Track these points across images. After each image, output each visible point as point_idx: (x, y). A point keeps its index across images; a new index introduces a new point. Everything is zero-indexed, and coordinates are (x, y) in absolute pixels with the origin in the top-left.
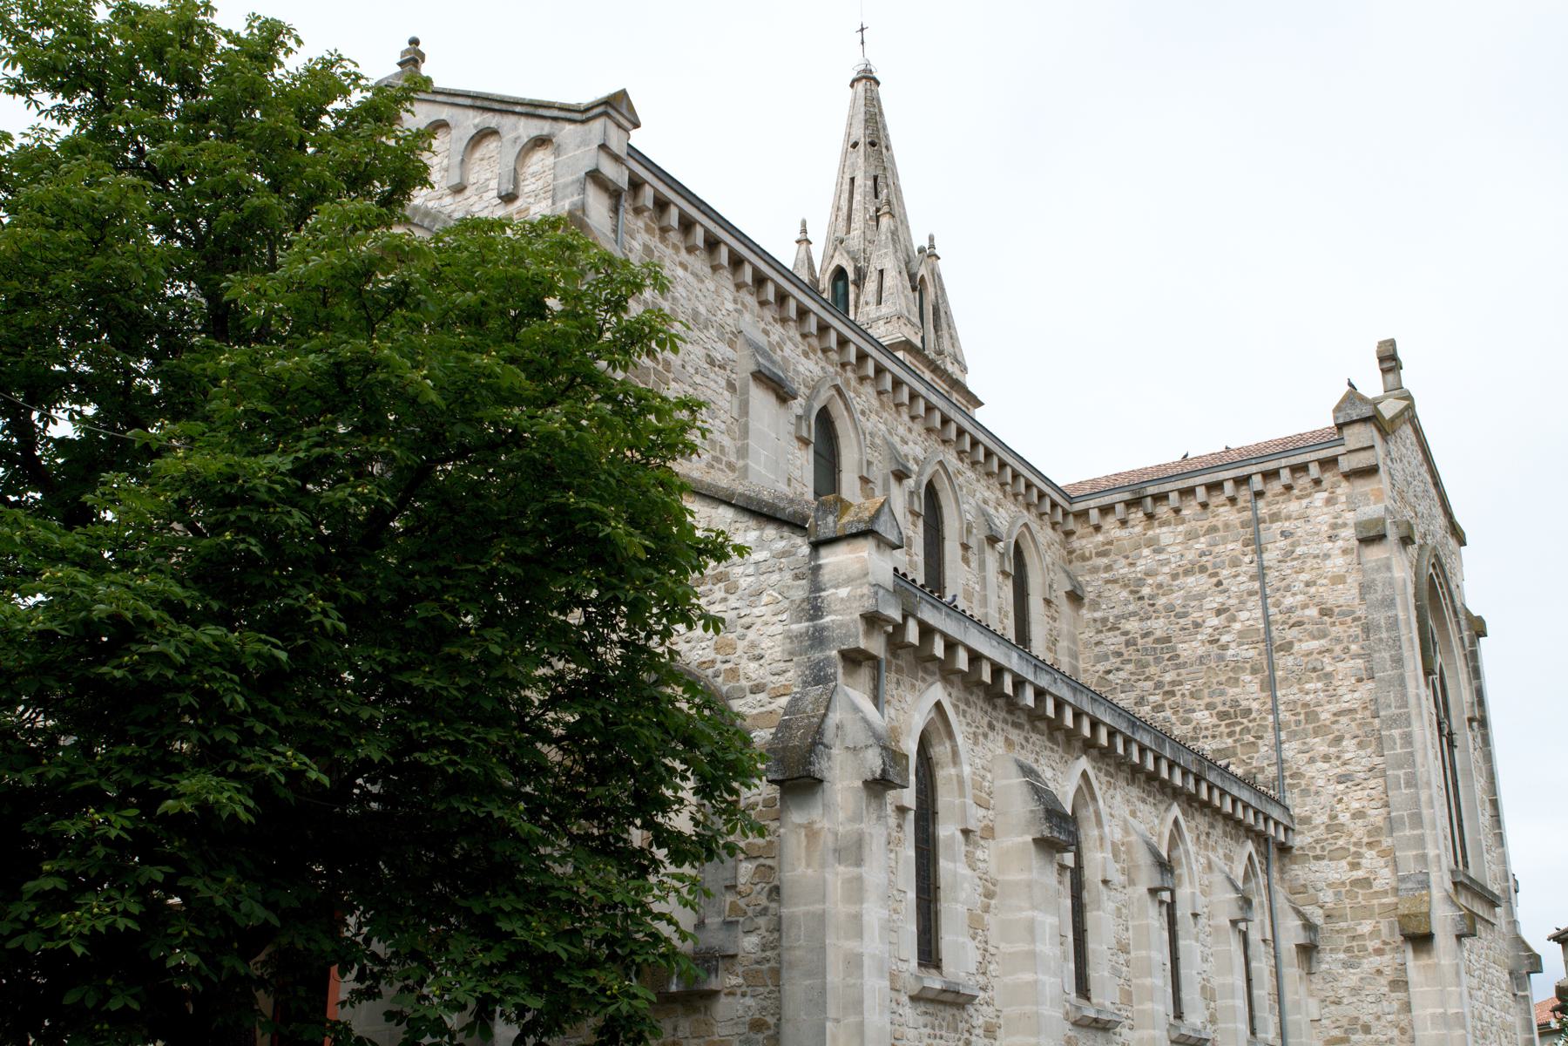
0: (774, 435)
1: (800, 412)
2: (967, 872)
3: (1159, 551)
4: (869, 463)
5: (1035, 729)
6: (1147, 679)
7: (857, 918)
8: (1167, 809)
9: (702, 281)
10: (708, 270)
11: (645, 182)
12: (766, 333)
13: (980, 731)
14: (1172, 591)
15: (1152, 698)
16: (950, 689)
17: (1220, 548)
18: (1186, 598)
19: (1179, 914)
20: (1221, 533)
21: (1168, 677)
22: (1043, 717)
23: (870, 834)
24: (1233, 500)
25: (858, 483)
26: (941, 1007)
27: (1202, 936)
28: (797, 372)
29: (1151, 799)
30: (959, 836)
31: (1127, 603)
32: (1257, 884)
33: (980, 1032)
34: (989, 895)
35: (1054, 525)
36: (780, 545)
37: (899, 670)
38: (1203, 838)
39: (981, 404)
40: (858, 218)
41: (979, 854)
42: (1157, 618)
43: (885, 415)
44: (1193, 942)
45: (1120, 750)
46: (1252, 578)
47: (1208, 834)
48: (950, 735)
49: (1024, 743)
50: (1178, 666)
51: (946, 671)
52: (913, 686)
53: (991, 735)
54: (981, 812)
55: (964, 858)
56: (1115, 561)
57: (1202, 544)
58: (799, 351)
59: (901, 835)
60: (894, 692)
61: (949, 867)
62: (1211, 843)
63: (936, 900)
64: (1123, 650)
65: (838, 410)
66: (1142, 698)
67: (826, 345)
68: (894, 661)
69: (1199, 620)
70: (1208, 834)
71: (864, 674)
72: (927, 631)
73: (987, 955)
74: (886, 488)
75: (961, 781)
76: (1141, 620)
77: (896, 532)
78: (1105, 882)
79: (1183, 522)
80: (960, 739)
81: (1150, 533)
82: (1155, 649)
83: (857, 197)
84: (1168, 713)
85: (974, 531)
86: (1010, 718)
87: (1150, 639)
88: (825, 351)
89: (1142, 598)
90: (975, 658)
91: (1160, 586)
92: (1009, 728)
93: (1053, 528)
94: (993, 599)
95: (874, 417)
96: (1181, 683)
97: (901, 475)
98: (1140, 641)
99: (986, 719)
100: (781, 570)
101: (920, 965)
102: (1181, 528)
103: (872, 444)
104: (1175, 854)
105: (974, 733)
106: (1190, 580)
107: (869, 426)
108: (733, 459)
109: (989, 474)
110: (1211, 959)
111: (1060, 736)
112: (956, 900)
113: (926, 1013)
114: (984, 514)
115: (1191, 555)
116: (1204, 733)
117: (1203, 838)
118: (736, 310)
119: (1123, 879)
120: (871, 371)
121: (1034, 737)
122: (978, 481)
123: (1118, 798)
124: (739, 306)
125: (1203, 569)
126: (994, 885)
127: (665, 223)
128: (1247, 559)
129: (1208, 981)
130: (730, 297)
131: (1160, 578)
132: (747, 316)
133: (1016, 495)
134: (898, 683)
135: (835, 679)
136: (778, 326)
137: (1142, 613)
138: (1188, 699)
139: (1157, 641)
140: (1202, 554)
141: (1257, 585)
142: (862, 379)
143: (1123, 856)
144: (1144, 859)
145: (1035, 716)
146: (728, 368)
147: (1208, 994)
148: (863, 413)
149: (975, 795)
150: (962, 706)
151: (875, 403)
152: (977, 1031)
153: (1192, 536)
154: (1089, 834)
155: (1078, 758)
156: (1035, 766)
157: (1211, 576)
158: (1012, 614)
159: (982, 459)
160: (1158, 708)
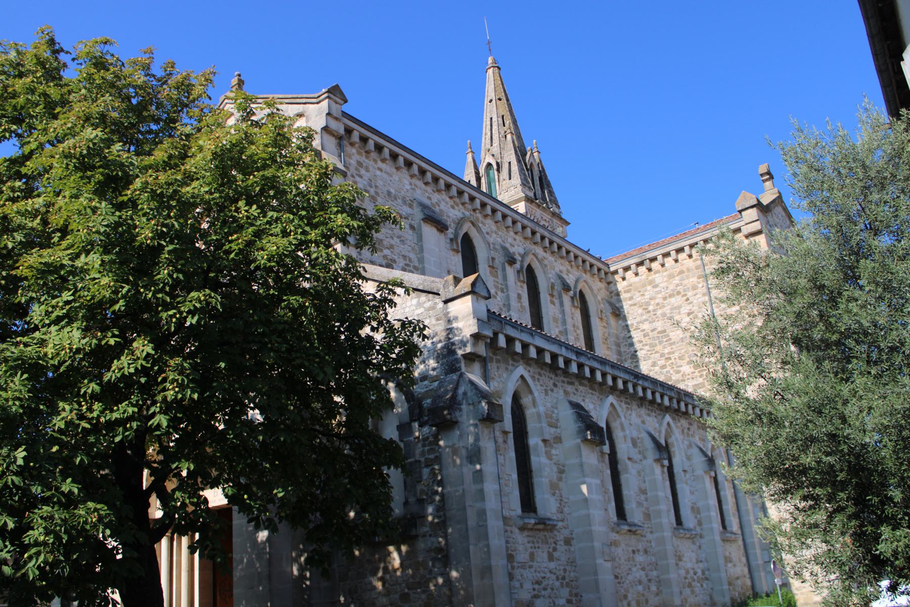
0: (437, 250)
1: (452, 236)
2: (547, 462)
3: (656, 286)
4: (493, 259)
5: (581, 384)
6: (656, 352)
7: (481, 491)
8: (663, 418)
9: (391, 176)
10: (394, 170)
11: (354, 129)
12: (429, 198)
13: (549, 388)
14: (664, 306)
15: (659, 363)
16: (528, 368)
17: (685, 282)
18: (671, 309)
19: (675, 471)
20: (686, 274)
21: (666, 351)
22: (584, 378)
23: (485, 447)
24: (690, 256)
25: (488, 269)
26: (538, 532)
27: (689, 482)
28: (449, 217)
29: (653, 414)
30: (541, 444)
31: (642, 315)
32: (720, 451)
33: (562, 543)
34: (561, 472)
35: (601, 280)
36: (428, 304)
37: (498, 361)
38: (686, 431)
39: (569, 224)
40: (496, 136)
41: (554, 452)
42: (658, 321)
43: (500, 233)
44: (684, 485)
45: (631, 390)
46: (704, 295)
47: (689, 429)
48: (531, 392)
49: (575, 392)
50: (671, 344)
51: (524, 357)
52: (507, 369)
53: (555, 390)
54: (553, 430)
55: (544, 455)
56: (634, 295)
57: (676, 280)
58: (449, 206)
59: (506, 446)
60: (496, 373)
61: (538, 460)
62: (691, 433)
63: (531, 477)
64: (643, 339)
65: (474, 234)
66: (655, 362)
67: (463, 201)
68: (494, 357)
69: (679, 320)
70: (689, 429)
71: (477, 366)
72: (510, 340)
73: (562, 503)
74: (504, 269)
75: (539, 415)
76: (650, 323)
77: (485, 291)
78: (629, 459)
79: (666, 270)
80: (536, 394)
81: (650, 278)
82: (658, 337)
83: (495, 127)
84: (668, 368)
85: (556, 287)
86: (566, 380)
87: (656, 332)
88: (463, 204)
89: (649, 312)
90: (540, 351)
91: (658, 304)
92: (566, 385)
93: (600, 281)
94: (569, 321)
95: (494, 235)
96: (673, 353)
97: (512, 261)
98: (651, 334)
99: (552, 382)
100: (430, 317)
101: (523, 511)
102: (665, 274)
103: (494, 248)
104: (670, 441)
105: (545, 390)
106: (673, 300)
107: (491, 240)
108: (417, 264)
109: (562, 257)
110: (696, 493)
111: (596, 386)
112: (541, 477)
113: (528, 536)
114: (560, 278)
115: (671, 287)
116: (688, 377)
117: (686, 431)
118: (412, 189)
119: (640, 457)
120: (489, 212)
121: (581, 388)
122: (556, 261)
123: (634, 414)
124: (413, 187)
125: (679, 293)
126: (564, 466)
127: (367, 149)
128: (700, 286)
129: (695, 504)
130: (407, 183)
131: (657, 301)
132: (418, 192)
133: (578, 267)
134: (498, 368)
135: (461, 369)
136: (436, 194)
137: (650, 319)
138: (678, 360)
139: (659, 333)
140: (677, 285)
141: (707, 298)
142: (486, 216)
143: (639, 445)
144: (649, 443)
145: (580, 376)
146: (410, 218)
147: (695, 510)
148: (488, 233)
149: (548, 422)
150: (537, 376)
151: (494, 228)
152: (560, 543)
153: (671, 277)
154: (618, 435)
155: (608, 396)
156: (582, 404)
157: (683, 296)
158: (581, 327)
159: (556, 250)
160: (663, 367)
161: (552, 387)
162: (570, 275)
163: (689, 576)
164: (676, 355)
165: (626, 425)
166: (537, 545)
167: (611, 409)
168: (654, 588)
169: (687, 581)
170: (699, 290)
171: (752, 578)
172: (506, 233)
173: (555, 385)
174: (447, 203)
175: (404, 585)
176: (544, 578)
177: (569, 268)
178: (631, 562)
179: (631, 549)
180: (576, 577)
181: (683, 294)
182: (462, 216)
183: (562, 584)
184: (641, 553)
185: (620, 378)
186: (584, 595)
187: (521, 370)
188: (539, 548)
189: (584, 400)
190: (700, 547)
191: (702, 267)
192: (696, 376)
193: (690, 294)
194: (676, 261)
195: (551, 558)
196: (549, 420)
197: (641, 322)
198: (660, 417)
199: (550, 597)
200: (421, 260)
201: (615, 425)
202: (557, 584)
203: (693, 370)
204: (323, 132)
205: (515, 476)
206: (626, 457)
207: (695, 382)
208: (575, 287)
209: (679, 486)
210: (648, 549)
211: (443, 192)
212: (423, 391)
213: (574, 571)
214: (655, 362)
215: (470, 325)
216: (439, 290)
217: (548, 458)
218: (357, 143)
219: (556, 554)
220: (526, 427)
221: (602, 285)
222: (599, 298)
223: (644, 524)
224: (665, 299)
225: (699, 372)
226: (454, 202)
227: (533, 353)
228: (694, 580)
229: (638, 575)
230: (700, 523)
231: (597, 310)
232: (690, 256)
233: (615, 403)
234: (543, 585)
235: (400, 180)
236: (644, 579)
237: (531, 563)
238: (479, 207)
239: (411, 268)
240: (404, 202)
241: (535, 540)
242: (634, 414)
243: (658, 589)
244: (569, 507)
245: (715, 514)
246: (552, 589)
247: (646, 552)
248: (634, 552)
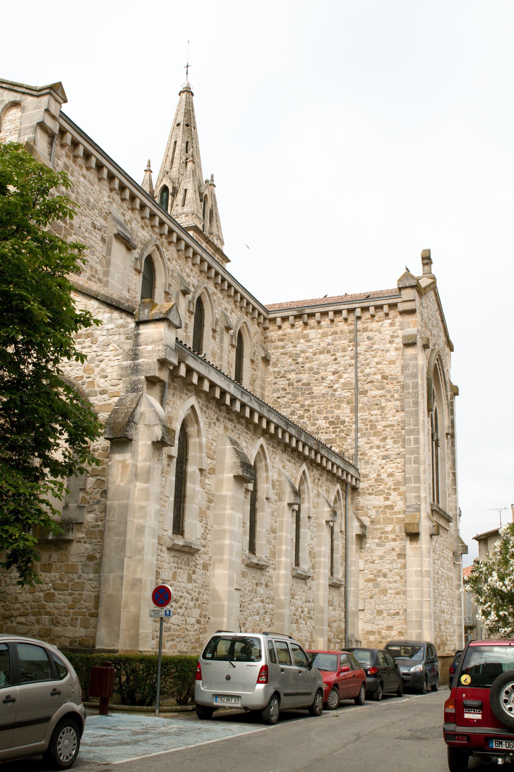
0: (123, 267)
1: (137, 256)
3: (308, 341)
4: (170, 285)
5: (239, 422)
6: (297, 403)
8: (300, 466)
9: (93, 185)
10: (96, 180)
12: (124, 215)
13: (212, 421)
15: (298, 412)
16: (199, 400)
17: (338, 342)
18: (319, 365)
20: (339, 335)
21: (307, 403)
22: (244, 417)
24: (346, 320)
29: (293, 461)
34: (210, 501)
35: (259, 324)
36: (120, 322)
37: (175, 388)
39: (229, 261)
40: (177, 162)
41: (207, 481)
42: (305, 373)
43: (180, 262)
44: (307, 530)
45: (280, 436)
46: (351, 358)
47: (319, 479)
48: (197, 422)
49: (234, 429)
50: (312, 398)
51: (198, 391)
52: (181, 397)
53: (217, 423)
55: (199, 483)
56: (287, 344)
57: (329, 339)
58: (139, 226)
59: (169, 469)
62: (320, 483)
63: (184, 502)
64: (287, 388)
65: (156, 257)
67: (153, 224)
68: (172, 384)
69: (325, 376)
70: (319, 479)
71: (157, 389)
73: (207, 530)
77: (178, 320)
78: (267, 499)
80: (202, 425)
81: (305, 332)
83: (177, 151)
84: (306, 420)
86: (227, 416)
87: (300, 383)
88: (152, 227)
89: (298, 363)
90: (213, 385)
91: (307, 358)
92: (226, 421)
93: (258, 325)
94: (225, 357)
95: (174, 262)
96: (313, 406)
98: (295, 384)
99: (216, 416)
100: (120, 334)
101: (173, 533)
102: (320, 331)
104: (302, 488)
105: (209, 422)
106: (322, 357)
109: (229, 296)
111: (251, 427)
112: (193, 503)
113: (175, 556)
114: (225, 315)
115: (323, 344)
117: (316, 481)
119: (276, 498)
121: (239, 426)
122: (223, 299)
123: (277, 459)
124: (111, 200)
125: (328, 352)
126: (213, 496)
127: (76, 154)
128: (350, 349)
129: (313, 549)
130: (107, 195)
132: (115, 205)
133: (241, 308)
134: (173, 395)
137: (297, 370)
138: (315, 414)
139: (303, 384)
140: (329, 344)
141: (353, 362)
142: (170, 243)
143: (277, 487)
145: (240, 416)
146: (103, 230)
148: (169, 260)
149: (207, 452)
150: (204, 409)
151: (175, 255)
153: (325, 335)
154: (261, 475)
155: (259, 438)
156: (238, 440)
157: (332, 355)
158: (234, 366)
159: (226, 288)
160: (301, 417)
161: (215, 421)
162: (233, 314)
163: (297, 613)
164: (316, 408)
165: (270, 468)
166: (180, 566)
167: (260, 450)
168: (268, 620)
169: (295, 617)
170: (348, 353)
171: (346, 622)
172: (185, 262)
173: (218, 420)
174: (138, 223)
175: (51, 585)
176: (181, 597)
177: (234, 307)
178: (253, 594)
179: (255, 581)
180: (208, 600)
181: (332, 353)
182: (149, 238)
183: (195, 604)
184: (263, 586)
185: (273, 423)
186: (211, 617)
187: (193, 400)
188: (181, 568)
189: (239, 438)
190: (310, 588)
191: (355, 332)
192: (330, 432)
193: (338, 354)
194: (332, 321)
195: (190, 580)
196: (208, 451)
197: (288, 371)
198: (298, 465)
199: (183, 615)
200: (106, 274)
201: (261, 466)
202: (191, 604)
203: (327, 425)
204: (38, 127)
205: (172, 499)
206: (265, 496)
207: (327, 437)
208: (236, 327)
209: (302, 530)
210: (269, 584)
211: (137, 211)
212: (101, 403)
213: (206, 594)
214: (294, 412)
215: (159, 350)
216: (134, 310)
217: (202, 487)
218: (68, 145)
219: (194, 577)
220: (187, 453)
221: (260, 330)
222: (254, 341)
223: (269, 560)
224: (315, 354)
225: (333, 428)
226: (145, 223)
227: (206, 386)
228: (301, 618)
229: (257, 605)
230: (313, 567)
231: (251, 352)
232: (346, 320)
233: (265, 446)
234: (179, 604)
235: (100, 191)
236: (262, 611)
237: (172, 582)
238: (166, 232)
239: (96, 280)
240: (100, 215)
241: (179, 561)
242: (277, 459)
243: (271, 621)
244: (211, 534)
245: (326, 560)
246: (186, 609)
247: (267, 586)
248: (257, 584)
